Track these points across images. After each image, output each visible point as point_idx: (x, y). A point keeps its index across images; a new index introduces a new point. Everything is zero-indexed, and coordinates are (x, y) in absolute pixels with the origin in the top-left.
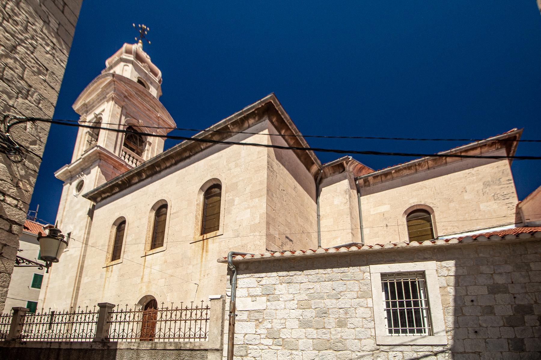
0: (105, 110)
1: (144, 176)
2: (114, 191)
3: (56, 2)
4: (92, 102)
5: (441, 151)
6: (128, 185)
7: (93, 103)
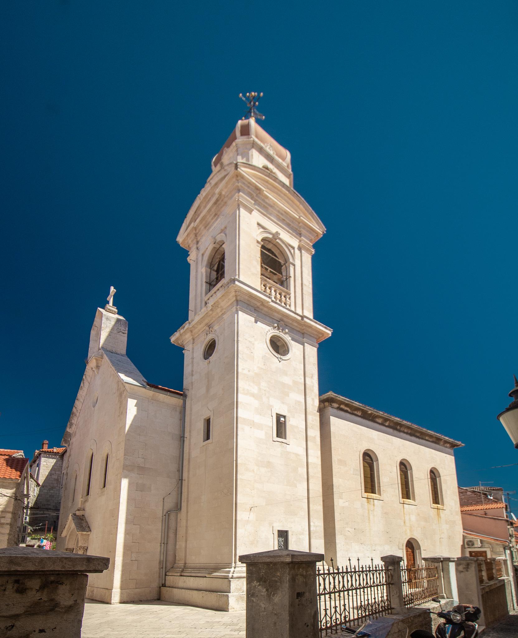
0: (218, 347)
1: (387, 424)
2: (356, 412)
5: (515, 515)
6: (371, 418)
7: (271, 206)
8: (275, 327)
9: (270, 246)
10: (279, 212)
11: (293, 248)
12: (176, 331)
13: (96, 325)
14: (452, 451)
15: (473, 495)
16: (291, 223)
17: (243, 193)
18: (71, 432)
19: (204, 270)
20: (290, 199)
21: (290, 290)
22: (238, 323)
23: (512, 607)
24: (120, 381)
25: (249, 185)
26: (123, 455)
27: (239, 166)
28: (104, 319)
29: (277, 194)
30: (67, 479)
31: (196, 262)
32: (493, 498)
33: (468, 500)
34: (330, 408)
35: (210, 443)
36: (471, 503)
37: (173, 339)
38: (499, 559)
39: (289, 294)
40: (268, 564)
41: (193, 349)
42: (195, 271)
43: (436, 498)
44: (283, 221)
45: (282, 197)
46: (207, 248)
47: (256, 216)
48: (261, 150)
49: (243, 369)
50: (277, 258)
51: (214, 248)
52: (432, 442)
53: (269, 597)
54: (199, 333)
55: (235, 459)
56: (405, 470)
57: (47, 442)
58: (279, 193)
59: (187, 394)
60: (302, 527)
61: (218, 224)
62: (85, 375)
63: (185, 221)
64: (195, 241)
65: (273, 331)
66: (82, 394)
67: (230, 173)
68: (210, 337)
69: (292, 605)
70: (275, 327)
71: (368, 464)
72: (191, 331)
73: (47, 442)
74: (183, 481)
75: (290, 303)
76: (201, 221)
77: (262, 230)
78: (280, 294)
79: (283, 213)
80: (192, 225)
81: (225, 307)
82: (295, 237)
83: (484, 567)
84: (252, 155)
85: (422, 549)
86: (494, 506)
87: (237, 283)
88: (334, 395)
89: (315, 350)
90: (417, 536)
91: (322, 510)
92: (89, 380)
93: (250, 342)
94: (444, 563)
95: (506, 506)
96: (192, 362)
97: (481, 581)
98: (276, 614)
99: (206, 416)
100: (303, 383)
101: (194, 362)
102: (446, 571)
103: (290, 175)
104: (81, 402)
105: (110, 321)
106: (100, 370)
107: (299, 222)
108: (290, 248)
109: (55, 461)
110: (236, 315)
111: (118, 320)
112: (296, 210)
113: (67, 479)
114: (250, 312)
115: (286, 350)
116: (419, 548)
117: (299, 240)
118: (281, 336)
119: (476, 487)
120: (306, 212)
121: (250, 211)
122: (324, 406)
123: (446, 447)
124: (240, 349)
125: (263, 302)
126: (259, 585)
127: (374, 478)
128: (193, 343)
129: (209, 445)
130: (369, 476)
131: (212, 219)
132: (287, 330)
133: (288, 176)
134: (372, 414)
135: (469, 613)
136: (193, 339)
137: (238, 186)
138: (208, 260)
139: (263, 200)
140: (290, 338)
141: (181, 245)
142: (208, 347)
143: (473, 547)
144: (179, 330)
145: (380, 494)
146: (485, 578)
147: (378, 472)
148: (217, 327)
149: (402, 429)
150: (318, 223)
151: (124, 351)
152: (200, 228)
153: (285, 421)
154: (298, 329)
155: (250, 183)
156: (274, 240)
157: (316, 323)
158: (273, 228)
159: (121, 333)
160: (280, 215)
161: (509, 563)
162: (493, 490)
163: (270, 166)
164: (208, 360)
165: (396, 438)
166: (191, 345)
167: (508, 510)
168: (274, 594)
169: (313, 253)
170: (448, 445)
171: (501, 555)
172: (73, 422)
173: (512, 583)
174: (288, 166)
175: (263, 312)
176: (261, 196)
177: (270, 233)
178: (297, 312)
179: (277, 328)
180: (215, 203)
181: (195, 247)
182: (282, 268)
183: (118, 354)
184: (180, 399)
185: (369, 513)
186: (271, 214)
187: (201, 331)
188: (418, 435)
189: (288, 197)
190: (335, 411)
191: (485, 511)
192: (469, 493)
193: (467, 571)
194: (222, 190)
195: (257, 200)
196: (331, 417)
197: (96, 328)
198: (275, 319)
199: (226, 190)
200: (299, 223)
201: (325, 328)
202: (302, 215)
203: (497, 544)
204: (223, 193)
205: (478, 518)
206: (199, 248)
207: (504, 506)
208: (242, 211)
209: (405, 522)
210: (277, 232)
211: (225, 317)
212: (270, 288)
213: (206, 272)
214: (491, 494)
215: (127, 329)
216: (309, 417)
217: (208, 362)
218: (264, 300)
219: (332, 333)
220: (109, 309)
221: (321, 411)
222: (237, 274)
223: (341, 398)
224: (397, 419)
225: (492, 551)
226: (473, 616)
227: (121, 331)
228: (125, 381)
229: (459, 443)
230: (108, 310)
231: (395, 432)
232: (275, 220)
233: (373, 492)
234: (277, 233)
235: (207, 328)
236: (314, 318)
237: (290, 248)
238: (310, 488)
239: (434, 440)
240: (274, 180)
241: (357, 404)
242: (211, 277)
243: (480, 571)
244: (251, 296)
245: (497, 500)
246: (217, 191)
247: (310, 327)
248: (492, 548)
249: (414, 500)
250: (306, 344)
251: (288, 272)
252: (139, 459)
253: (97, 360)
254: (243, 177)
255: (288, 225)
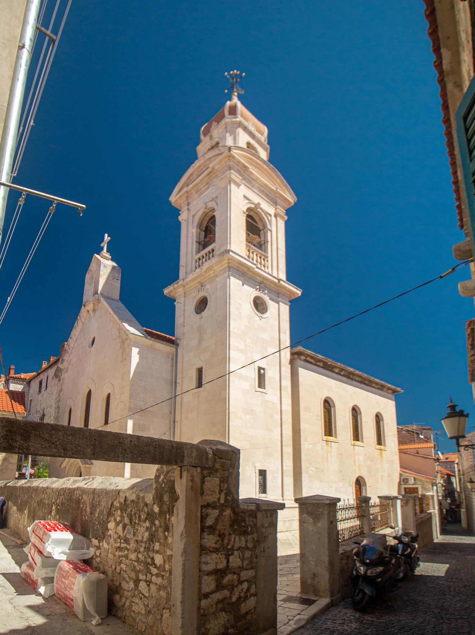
1: (342, 373)
2: (318, 364)
3: (474, 428)
4: (254, 178)
6: (330, 368)
7: (254, 180)
8: (257, 289)
9: (252, 214)
10: (260, 184)
11: (271, 215)
12: (170, 285)
13: (91, 270)
14: (393, 397)
15: (407, 435)
16: (269, 194)
17: (234, 171)
18: (62, 368)
19: (194, 230)
20: (269, 173)
21: (267, 254)
22: (229, 287)
23: (436, 536)
24: (126, 332)
25: (238, 164)
26: (129, 398)
27: (231, 149)
28: (102, 267)
29: (259, 169)
30: (58, 412)
31: (187, 221)
32: (424, 437)
33: (403, 439)
34: (298, 360)
35: (202, 391)
36: (405, 441)
37: (166, 291)
38: (428, 495)
39: (267, 257)
40: (313, 504)
41: (185, 302)
42: (186, 230)
43: (380, 440)
44: (263, 192)
45: (263, 172)
46: (198, 211)
47: (243, 190)
48: (245, 129)
49: (234, 328)
50: (256, 222)
51: (205, 212)
52: (378, 389)
53: (315, 523)
54: (191, 288)
55: (227, 408)
56: (355, 414)
57: (14, 367)
58: (261, 168)
59: (179, 343)
60: (276, 466)
61: (210, 193)
62: (80, 315)
63: (178, 184)
64: (186, 202)
65: (256, 292)
66: (76, 332)
67: (224, 154)
68: (202, 294)
69: (329, 528)
70: (257, 289)
71: (327, 410)
72: (184, 287)
73: (14, 367)
74: (176, 423)
75: (268, 265)
76: (193, 188)
77: (247, 201)
78: (260, 258)
79: (264, 185)
80: (185, 189)
81: (217, 271)
82: (272, 205)
83: (417, 503)
84: (238, 133)
85: (368, 485)
86: (425, 445)
87: (231, 253)
88: (303, 350)
89: (288, 307)
90: (365, 475)
91: (292, 452)
92: (83, 320)
93: (238, 303)
94: (393, 500)
95: (435, 445)
96: (184, 314)
97: (416, 514)
98: (319, 533)
99: (199, 366)
100: (278, 338)
101: (185, 315)
102: (394, 506)
103: (267, 148)
104: (74, 340)
105: (107, 268)
106: (96, 313)
107: (276, 193)
108: (268, 215)
109: (22, 388)
110: (228, 280)
111: (114, 267)
112: (273, 182)
113: (58, 412)
114: (238, 276)
115: (264, 308)
116: (365, 485)
117: (275, 208)
118: (261, 296)
119: (410, 426)
120: (281, 184)
121: (238, 185)
122: (294, 357)
123: (389, 393)
124: (231, 310)
125: (249, 268)
126: (308, 516)
127: (331, 422)
128: (185, 297)
129: (202, 392)
130: (327, 420)
131: (204, 187)
132: (266, 292)
133: (266, 150)
134: (331, 365)
135: (413, 536)
136: (185, 293)
137: (229, 165)
138: (199, 221)
139: (248, 175)
140: (268, 298)
141: (173, 204)
142: (199, 302)
143: (407, 483)
144: (173, 284)
145: (336, 437)
146: (418, 511)
147: (335, 417)
148: (209, 287)
149: (354, 378)
150: (290, 194)
151: (117, 297)
152: (192, 192)
153: (264, 373)
154: (275, 290)
155: (239, 162)
156: (256, 209)
157: (289, 285)
158: (256, 199)
159: (115, 280)
160: (261, 188)
161: (435, 498)
162: (424, 429)
163: (252, 142)
164: (201, 315)
165: (350, 386)
166: (183, 298)
167: (436, 448)
168: (318, 522)
169: (286, 219)
170: (390, 391)
171: (429, 491)
172: (65, 358)
173: (437, 515)
174: (265, 140)
175: (248, 276)
176: (247, 172)
177: (253, 204)
178: (274, 275)
179: (258, 290)
180: (208, 175)
181: (186, 207)
182: (261, 232)
183: (114, 300)
184: (173, 347)
185: (327, 454)
186: (253, 186)
187: (193, 287)
188: (367, 382)
189: (267, 172)
190: (302, 363)
191: (417, 449)
192: (404, 432)
193: (407, 506)
194: (215, 165)
195: (244, 176)
196: (300, 369)
197: (91, 272)
198: (257, 282)
199: (218, 166)
200: (276, 194)
201: (296, 289)
202: (279, 187)
203: (427, 482)
204: (216, 168)
205: (412, 456)
206: (190, 209)
207: (433, 446)
208: (233, 186)
209: (355, 462)
210: (259, 203)
211: (218, 279)
212: (253, 253)
213: (197, 233)
214: (422, 433)
215: (120, 275)
216: (283, 369)
217: (200, 317)
218: (250, 266)
219: (302, 293)
220: (104, 256)
221: (292, 362)
222: (229, 242)
223: (309, 352)
224: (351, 369)
225: (423, 488)
226: (414, 539)
227: (115, 278)
228: (131, 332)
229: (399, 389)
230: (103, 257)
231: (349, 381)
232: (257, 192)
233: (330, 435)
234: (259, 204)
235: (200, 286)
236: (287, 280)
237: (268, 215)
238: (283, 432)
239: (379, 386)
240: (257, 159)
241: (320, 357)
242: (200, 236)
243: (415, 505)
244: (240, 263)
245: (427, 440)
246: (211, 166)
247: (285, 288)
248: (423, 485)
249: (362, 442)
250: (280, 303)
251: (266, 237)
252: (141, 402)
253: (94, 304)
254: (234, 157)
255: (267, 195)
